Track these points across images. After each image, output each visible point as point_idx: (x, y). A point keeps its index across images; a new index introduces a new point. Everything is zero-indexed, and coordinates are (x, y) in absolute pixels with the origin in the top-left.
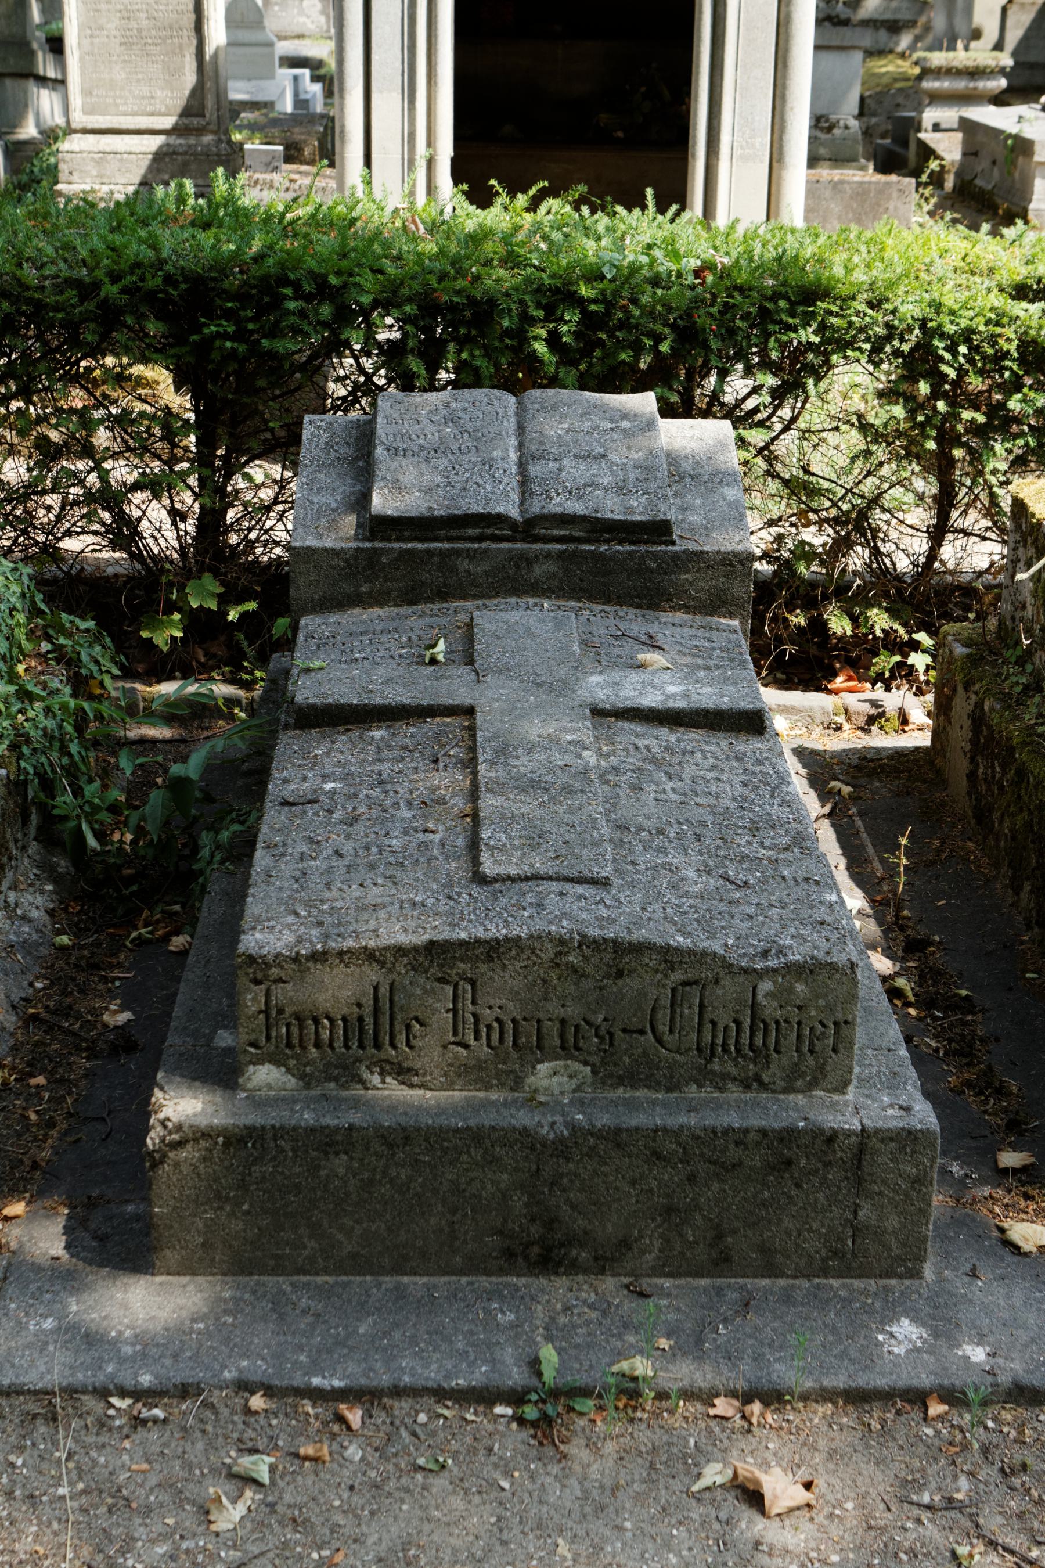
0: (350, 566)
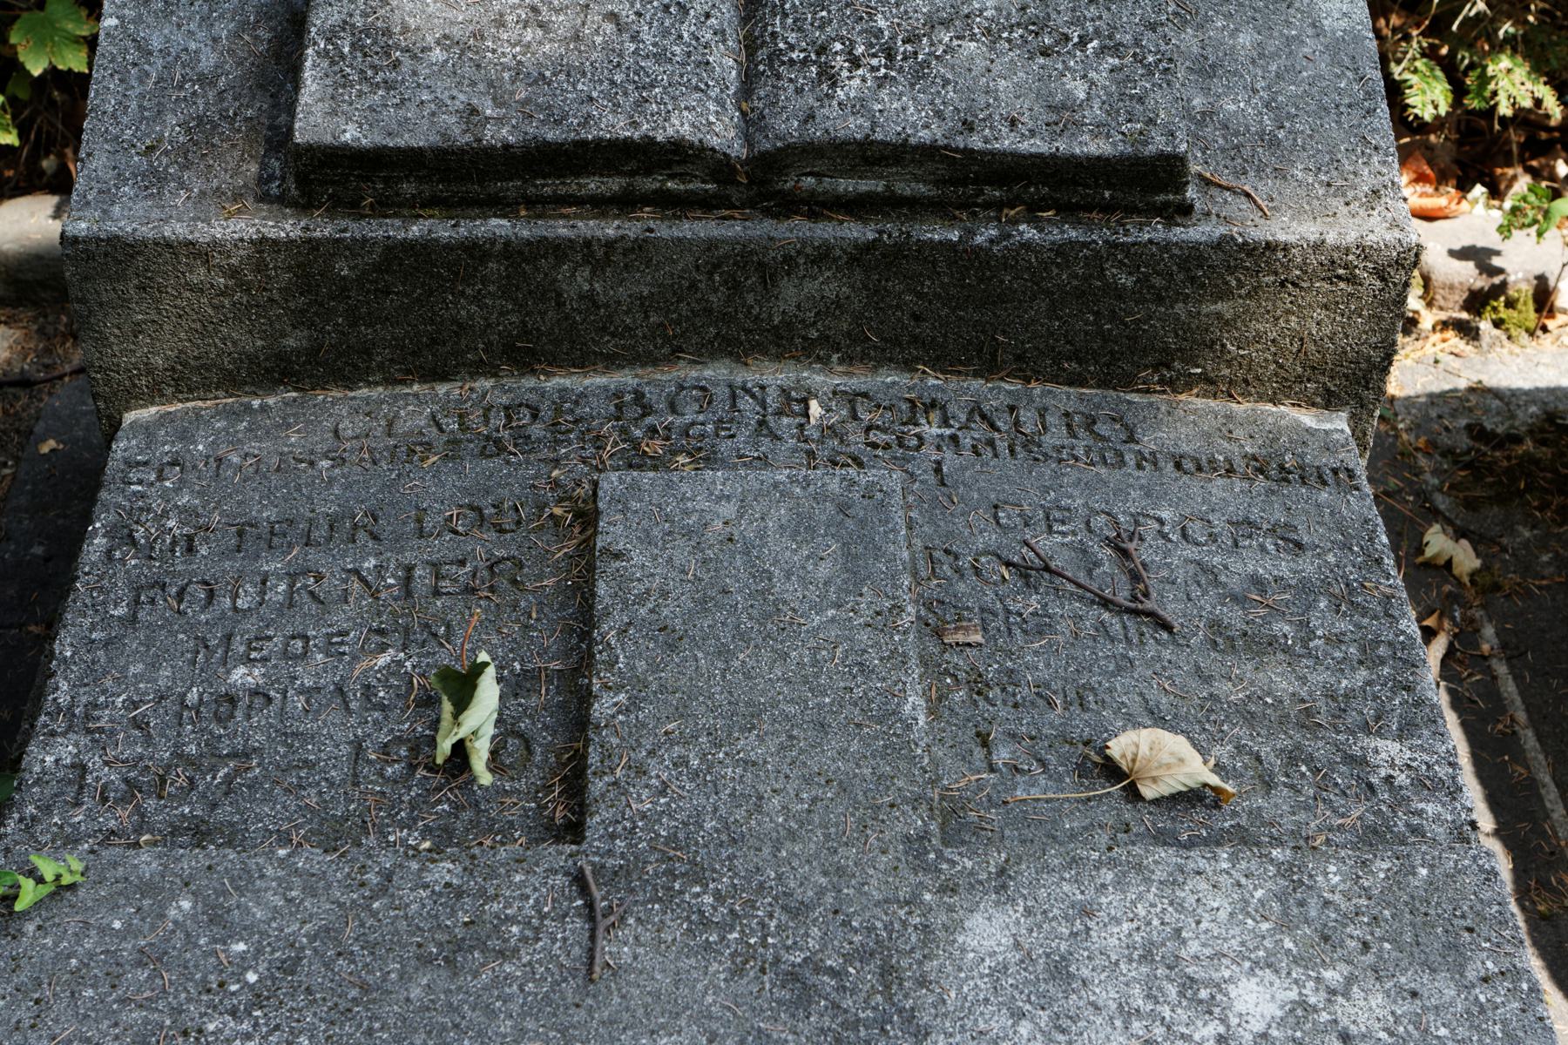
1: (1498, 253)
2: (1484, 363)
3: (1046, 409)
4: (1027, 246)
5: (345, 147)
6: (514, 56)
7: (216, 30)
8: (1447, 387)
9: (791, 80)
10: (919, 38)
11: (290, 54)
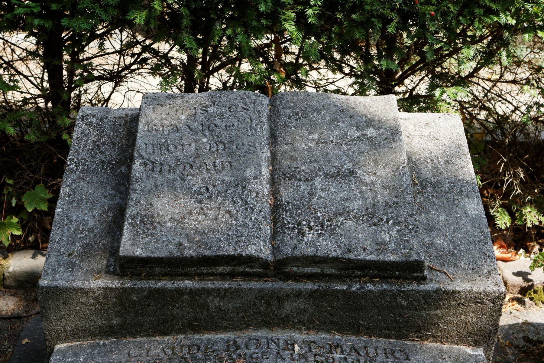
0: (100, 303)
1: (530, 274)
2: (527, 314)
3: (377, 347)
4: (370, 291)
5: (137, 257)
6: (195, 225)
7: (94, 213)
8: (515, 322)
9: (289, 234)
10: (332, 220)
11: (119, 222)
